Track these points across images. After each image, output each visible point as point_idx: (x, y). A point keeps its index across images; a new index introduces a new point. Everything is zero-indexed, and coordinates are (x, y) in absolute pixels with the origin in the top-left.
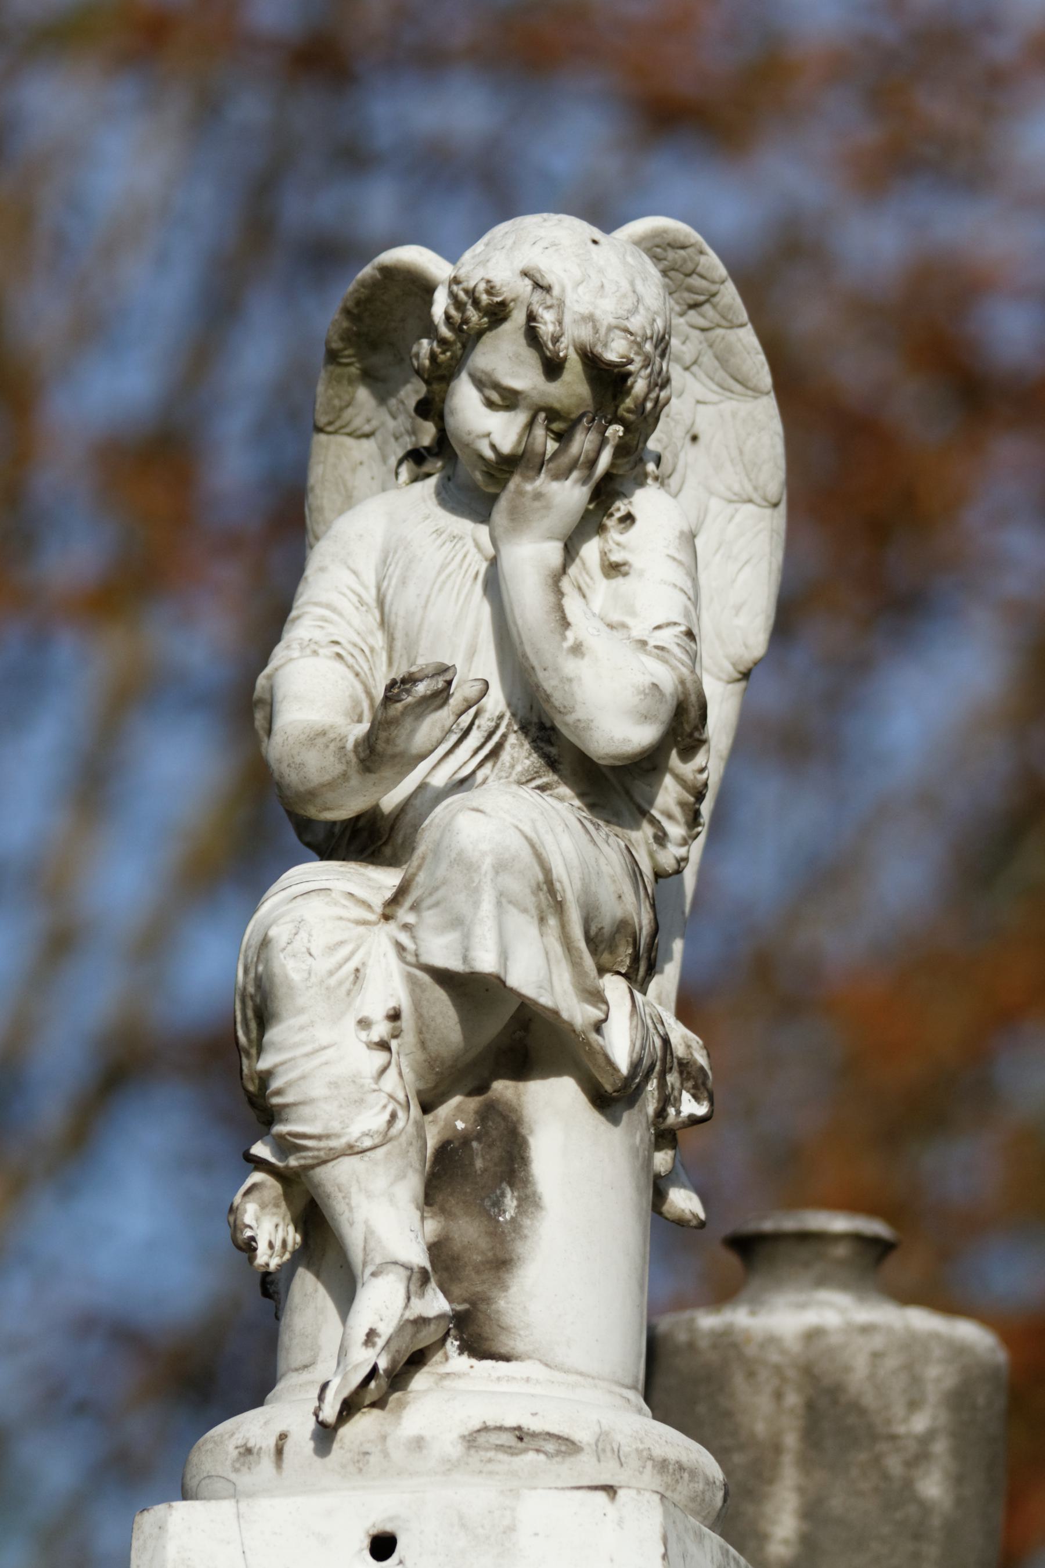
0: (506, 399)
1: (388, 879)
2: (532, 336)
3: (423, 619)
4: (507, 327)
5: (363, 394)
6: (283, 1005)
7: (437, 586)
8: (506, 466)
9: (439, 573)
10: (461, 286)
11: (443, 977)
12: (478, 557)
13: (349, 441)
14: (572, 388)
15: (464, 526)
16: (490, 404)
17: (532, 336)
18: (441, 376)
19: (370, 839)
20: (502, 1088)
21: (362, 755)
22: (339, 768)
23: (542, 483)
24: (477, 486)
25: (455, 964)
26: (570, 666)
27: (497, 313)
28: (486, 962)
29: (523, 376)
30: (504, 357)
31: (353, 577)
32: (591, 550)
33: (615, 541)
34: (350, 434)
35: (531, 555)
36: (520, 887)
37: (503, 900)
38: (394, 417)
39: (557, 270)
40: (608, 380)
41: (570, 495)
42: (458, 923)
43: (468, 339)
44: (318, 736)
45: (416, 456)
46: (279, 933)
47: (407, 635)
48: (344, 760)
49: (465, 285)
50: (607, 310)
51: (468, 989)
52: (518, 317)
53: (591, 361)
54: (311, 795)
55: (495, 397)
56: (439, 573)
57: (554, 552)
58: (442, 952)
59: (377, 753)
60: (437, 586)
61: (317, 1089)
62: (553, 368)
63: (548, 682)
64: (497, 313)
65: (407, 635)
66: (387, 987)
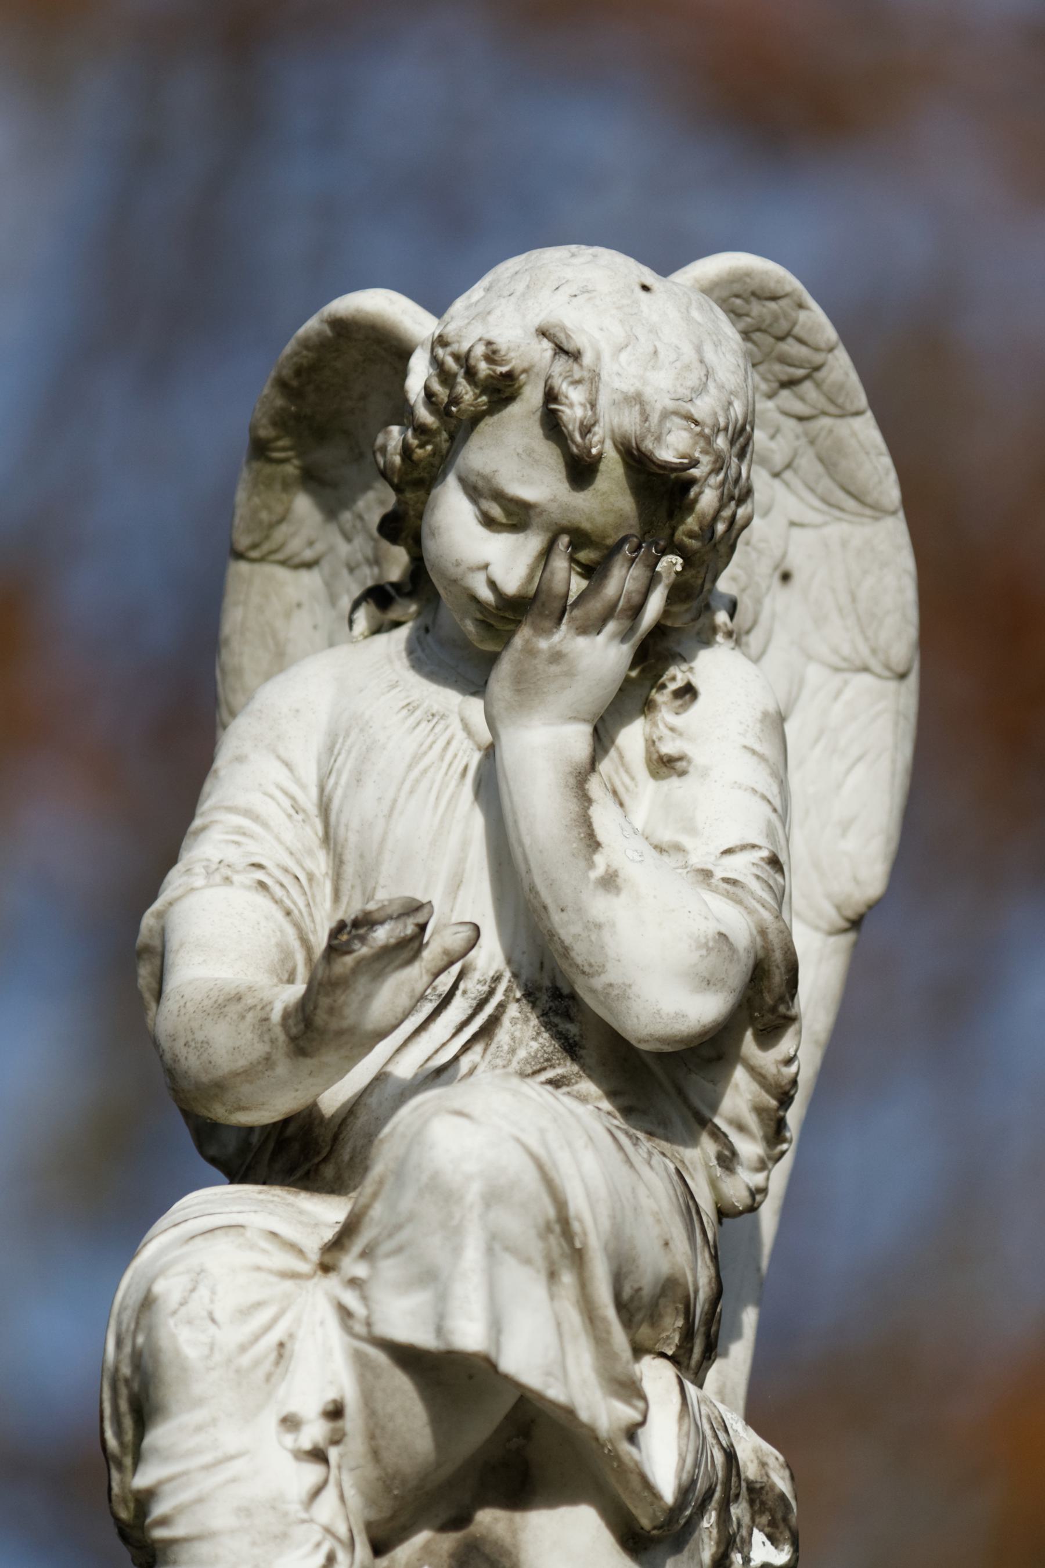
0: (512, 515)
1: (328, 1212)
2: (552, 423)
3: (385, 833)
4: (515, 409)
5: (303, 504)
6: (172, 1392)
7: (407, 786)
8: (511, 612)
9: (410, 767)
10: (449, 349)
11: (406, 1357)
12: (468, 744)
13: (282, 574)
14: (609, 500)
15: (447, 699)
16: (488, 522)
17: (552, 423)
18: (417, 480)
19: (303, 1153)
20: (489, 1520)
21: (294, 1031)
22: (261, 1049)
23: (563, 637)
24: (468, 641)
25: (423, 1338)
26: (600, 906)
27: (502, 390)
28: (469, 1335)
29: (540, 483)
30: (511, 454)
31: (284, 770)
32: (632, 737)
33: (668, 725)
34: (283, 563)
35: (544, 743)
36: (520, 1226)
37: (496, 1245)
38: (348, 539)
39: (590, 327)
40: (662, 489)
41: (601, 657)
42: (430, 1277)
43: (457, 426)
44: (229, 1002)
45: (380, 596)
46: (169, 1289)
47: (362, 856)
48: (266, 1038)
49: (454, 347)
50: (662, 386)
51: (444, 1376)
52: (532, 396)
53: (637, 461)
54: (219, 1088)
55: (496, 511)
56: (410, 767)
57: (577, 739)
58: (406, 1320)
59: (315, 1028)
60: (407, 786)
61: (219, 1517)
62: (581, 470)
63: (567, 928)
64: (502, 390)
65: (362, 856)
66: (324, 1369)
